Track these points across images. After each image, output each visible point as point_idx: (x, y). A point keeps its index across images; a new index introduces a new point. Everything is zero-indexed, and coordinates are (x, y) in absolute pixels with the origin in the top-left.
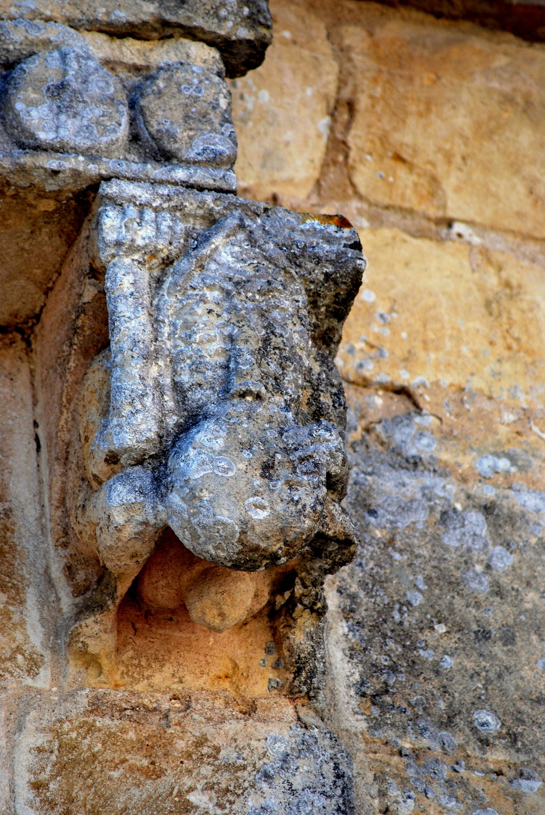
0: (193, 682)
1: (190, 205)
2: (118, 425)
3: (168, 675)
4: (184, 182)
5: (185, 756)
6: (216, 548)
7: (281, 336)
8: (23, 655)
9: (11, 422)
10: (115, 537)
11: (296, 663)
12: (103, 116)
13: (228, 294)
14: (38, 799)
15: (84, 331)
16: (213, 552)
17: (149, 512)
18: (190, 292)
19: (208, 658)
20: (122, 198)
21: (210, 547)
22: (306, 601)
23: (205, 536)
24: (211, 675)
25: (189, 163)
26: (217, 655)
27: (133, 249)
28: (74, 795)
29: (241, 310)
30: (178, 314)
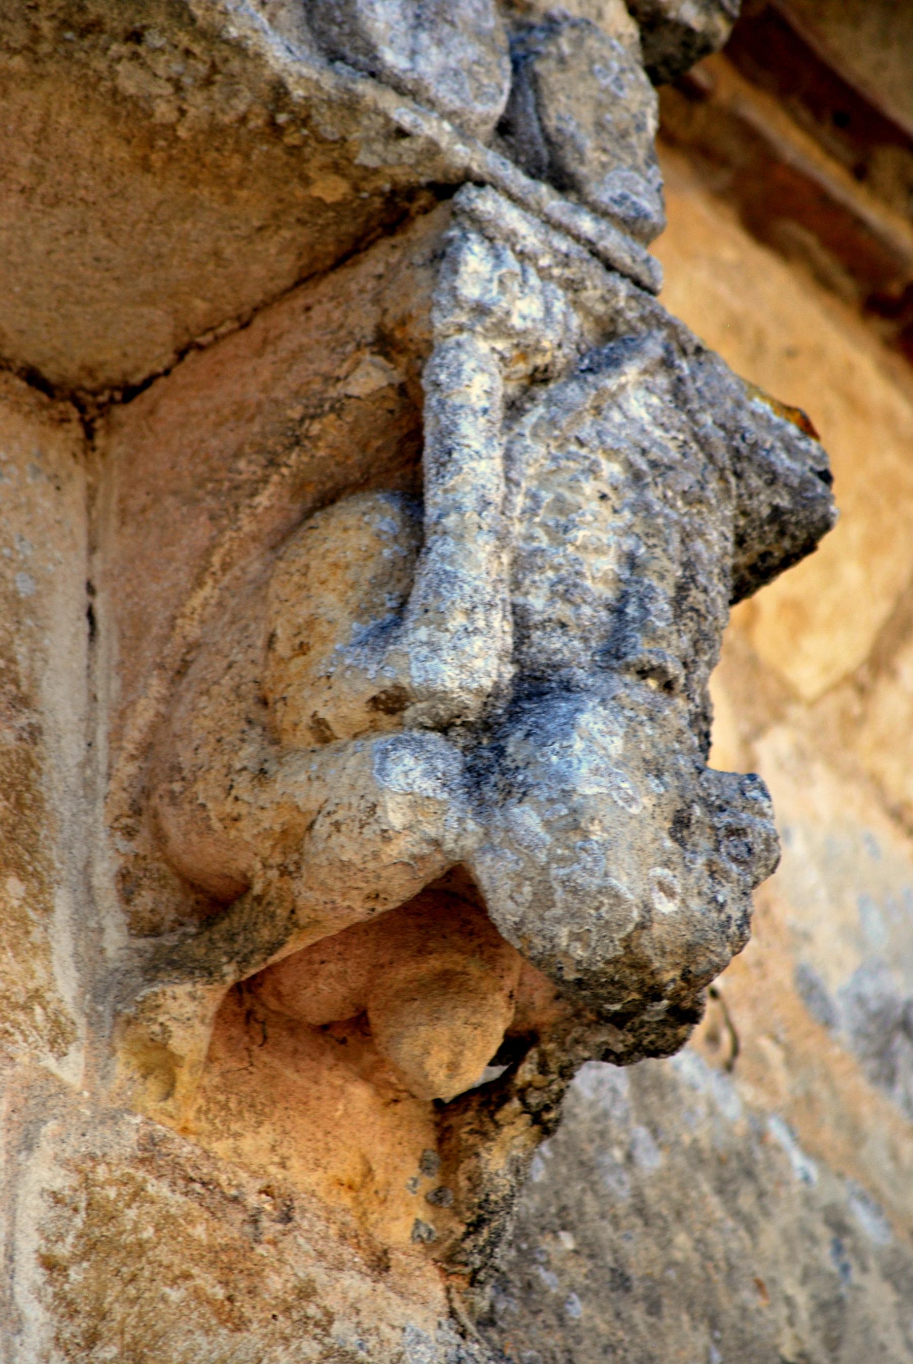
0: (302, 1177)
2: (429, 643)
5: (282, 1308)
6: (575, 937)
8: (44, 1008)
9: (50, 567)
10: (370, 848)
11: (480, 1207)
12: (478, 63)
13: (637, 477)
14: (50, 1290)
15: (316, 447)
16: (564, 942)
17: (456, 829)
18: (573, 448)
19: (330, 1139)
20: (497, 226)
21: (563, 934)
22: (534, 1099)
23: (567, 908)
24: (331, 1173)
25: (600, 212)
27: (502, 329)
28: (106, 1306)
29: (658, 515)
30: (544, 479)
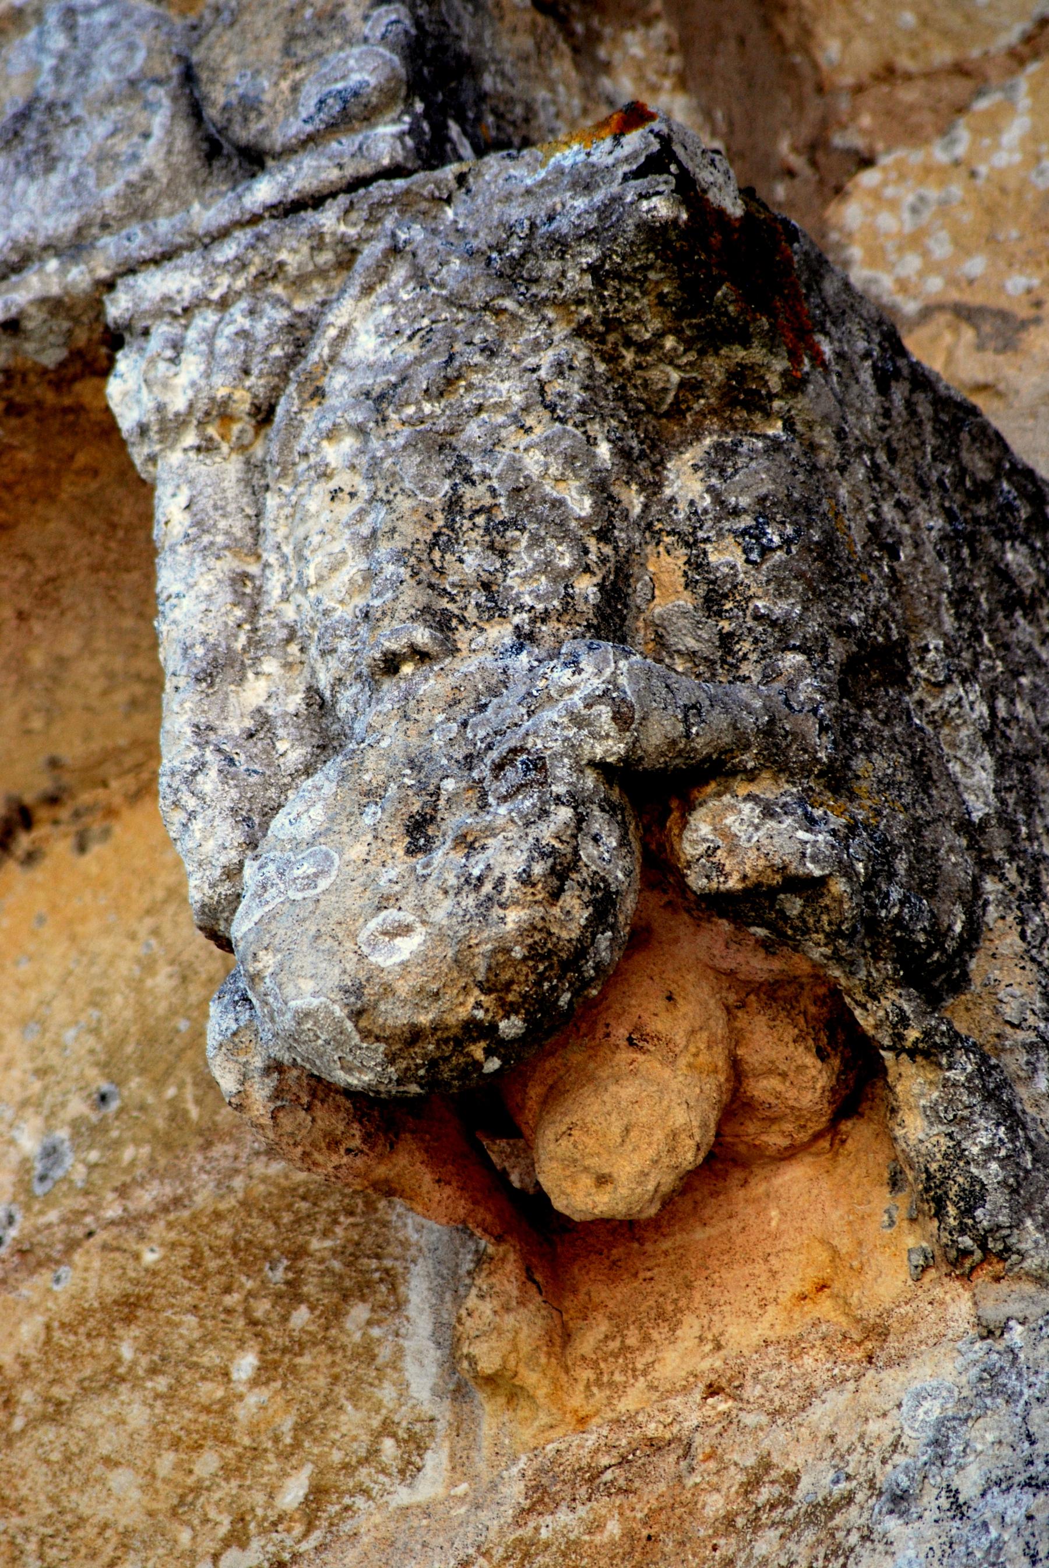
0: (742, 1334)
1: (293, 256)
3: (691, 1343)
4: (273, 206)
7: (485, 476)
24: (783, 1298)
26: (791, 1244)
